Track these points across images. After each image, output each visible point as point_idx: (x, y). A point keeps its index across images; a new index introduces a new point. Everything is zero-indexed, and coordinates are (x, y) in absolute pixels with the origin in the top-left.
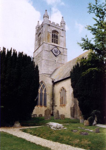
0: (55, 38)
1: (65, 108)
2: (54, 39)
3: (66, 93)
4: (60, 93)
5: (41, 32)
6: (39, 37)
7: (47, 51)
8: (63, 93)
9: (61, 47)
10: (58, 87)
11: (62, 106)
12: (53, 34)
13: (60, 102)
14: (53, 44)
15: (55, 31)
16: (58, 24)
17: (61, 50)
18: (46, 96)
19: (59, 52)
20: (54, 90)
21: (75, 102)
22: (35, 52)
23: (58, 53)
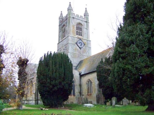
0: (79, 30)
1: (91, 96)
2: (78, 31)
3: (92, 84)
4: (87, 84)
5: (66, 24)
6: (63, 29)
7: (72, 44)
8: (89, 84)
9: (85, 39)
10: (85, 79)
11: (89, 95)
12: (77, 27)
13: (87, 92)
14: (77, 36)
15: (80, 24)
16: (81, 17)
17: (85, 41)
18: (75, 87)
19: (83, 44)
20: (81, 82)
21: (99, 91)
22: (60, 43)
23: (83, 46)
